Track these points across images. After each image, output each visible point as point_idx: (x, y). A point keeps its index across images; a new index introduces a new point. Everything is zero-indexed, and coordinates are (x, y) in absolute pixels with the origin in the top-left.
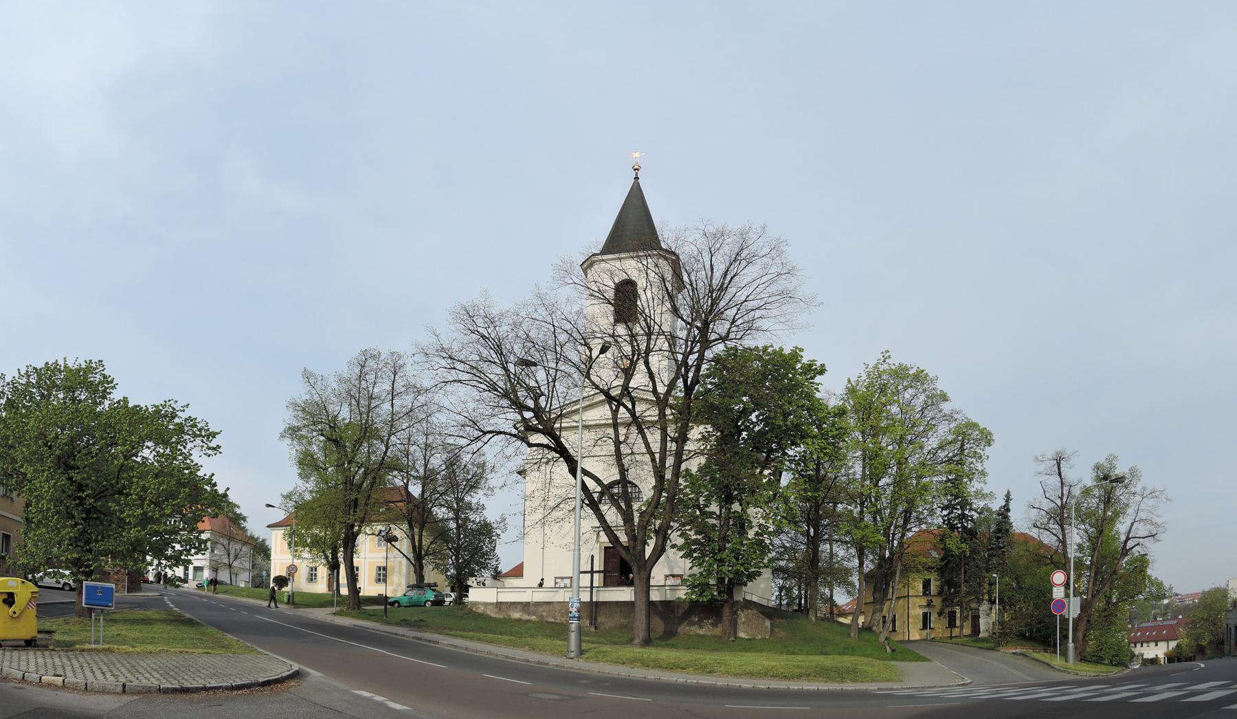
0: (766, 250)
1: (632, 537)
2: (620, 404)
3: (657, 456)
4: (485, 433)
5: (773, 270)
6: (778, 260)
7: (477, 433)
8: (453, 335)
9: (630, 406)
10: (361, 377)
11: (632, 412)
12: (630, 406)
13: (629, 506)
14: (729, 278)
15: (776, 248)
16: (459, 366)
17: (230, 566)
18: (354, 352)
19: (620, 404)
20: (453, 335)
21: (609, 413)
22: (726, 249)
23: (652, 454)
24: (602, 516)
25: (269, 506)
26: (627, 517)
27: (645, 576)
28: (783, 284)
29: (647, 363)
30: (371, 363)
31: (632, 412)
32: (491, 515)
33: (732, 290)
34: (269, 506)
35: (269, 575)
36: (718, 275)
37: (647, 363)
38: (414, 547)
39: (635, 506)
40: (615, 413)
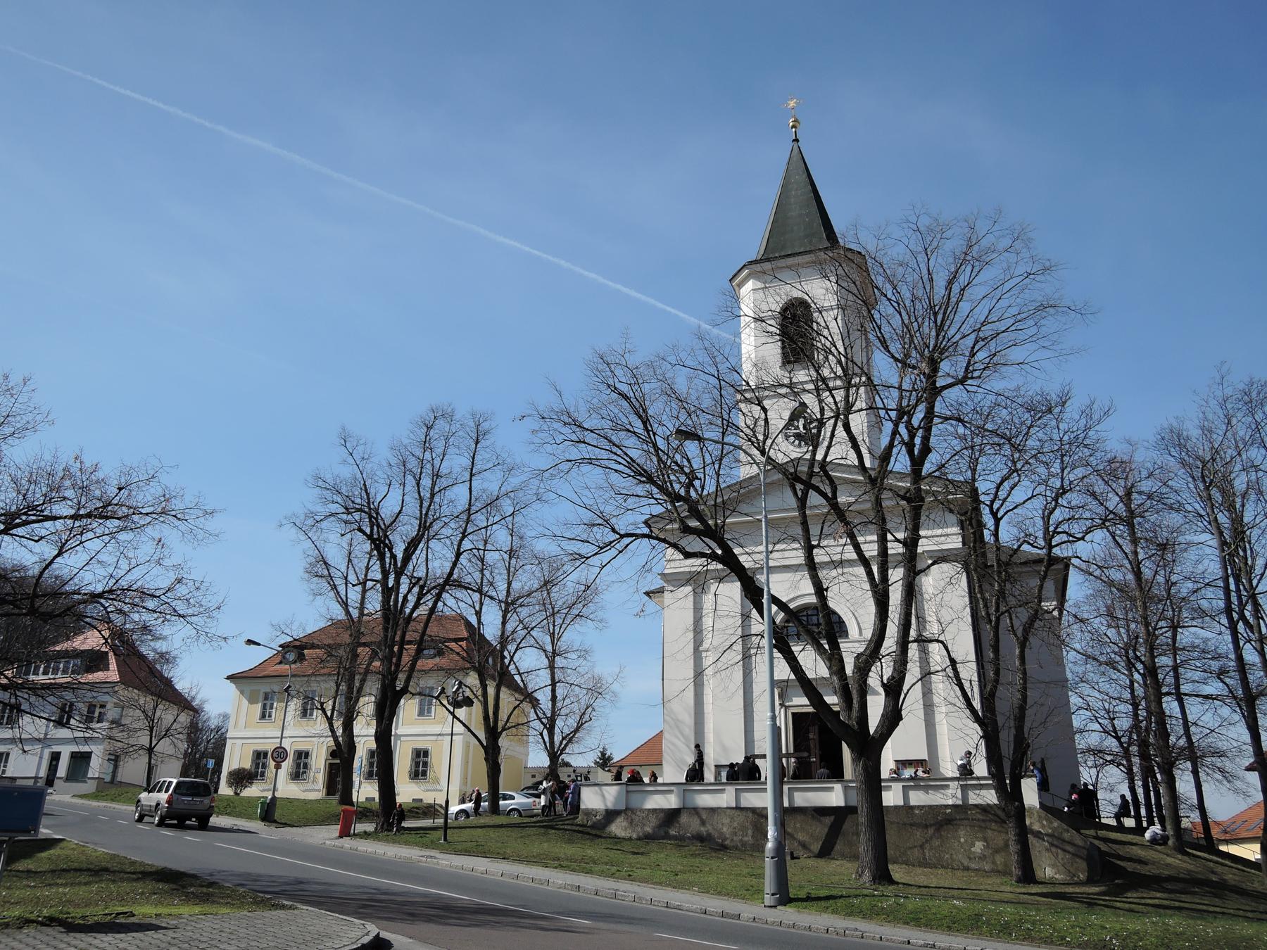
0: (1006, 242)
1: (845, 693)
2: (809, 486)
3: (875, 569)
4: (622, 536)
5: (1021, 270)
6: (1025, 254)
7: (613, 537)
8: (580, 392)
9: (828, 490)
10: (426, 445)
11: (832, 502)
12: (828, 490)
13: (835, 646)
14: (956, 289)
15: (1019, 236)
16: (590, 437)
17: (150, 750)
18: (421, 410)
19: (809, 486)
20: (580, 392)
21: (793, 502)
22: (948, 246)
23: (865, 562)
24: (795, 659)
25: (250, 642)
26: (834, 659)
27: (1060, 576)
28: (1039, 291)
29: (847, 427)
30: (441, 424)
31: (832, 502)
32: (603, 666)
33: (964, 307)
34: (250, 642)
35: (219, 764)
36: (940, 291)
37: (847, 427)
38: (486, 718)
39: (844, 646)
40: (802, 503)
